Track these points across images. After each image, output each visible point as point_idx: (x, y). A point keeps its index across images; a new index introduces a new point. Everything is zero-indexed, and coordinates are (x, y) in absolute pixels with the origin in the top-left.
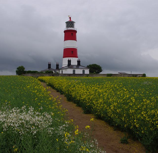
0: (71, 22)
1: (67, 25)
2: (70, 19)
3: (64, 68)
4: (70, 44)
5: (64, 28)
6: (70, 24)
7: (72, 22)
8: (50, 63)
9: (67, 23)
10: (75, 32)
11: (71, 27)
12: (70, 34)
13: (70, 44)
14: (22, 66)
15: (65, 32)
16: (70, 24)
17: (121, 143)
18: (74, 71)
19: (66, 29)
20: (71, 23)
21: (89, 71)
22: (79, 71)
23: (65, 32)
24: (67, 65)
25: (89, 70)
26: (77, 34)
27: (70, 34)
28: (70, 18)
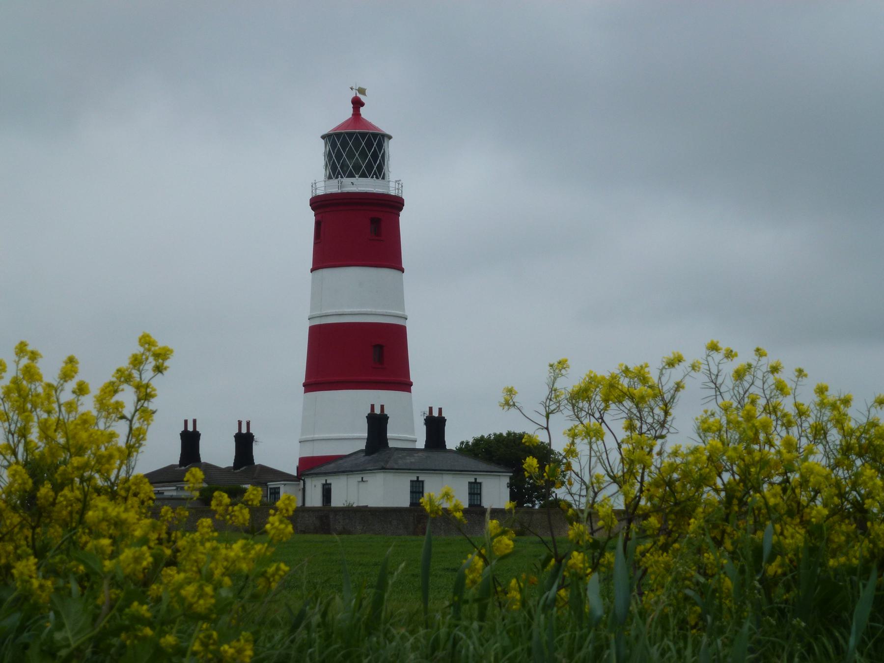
0: (363, 135)
1: (339, 156)
2: (356, 113)
3: (609, 469)
4: (356, 296)
5: (308, 172)
6: (357, 146)
7: (375, 135)
8: (248, 424)
9: (334, 145)
10: (393, 205)
11: (363, 175)
12: (357, 227)
13: (356, 296)
14: (462, 443)
15: (319, 204)
16: (357, 146)
17: (37, 469)
18: (417, 489)
19: (325, 187)
20: (369, 145)
21: (510, 486)
22: (447, 491)
23: (319, 204)
24: (362, 445)
25: (507, 480)
26: (405, 219)
27: (357, 227)
28: (357, 104)
